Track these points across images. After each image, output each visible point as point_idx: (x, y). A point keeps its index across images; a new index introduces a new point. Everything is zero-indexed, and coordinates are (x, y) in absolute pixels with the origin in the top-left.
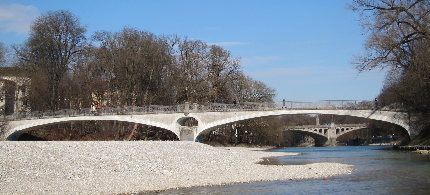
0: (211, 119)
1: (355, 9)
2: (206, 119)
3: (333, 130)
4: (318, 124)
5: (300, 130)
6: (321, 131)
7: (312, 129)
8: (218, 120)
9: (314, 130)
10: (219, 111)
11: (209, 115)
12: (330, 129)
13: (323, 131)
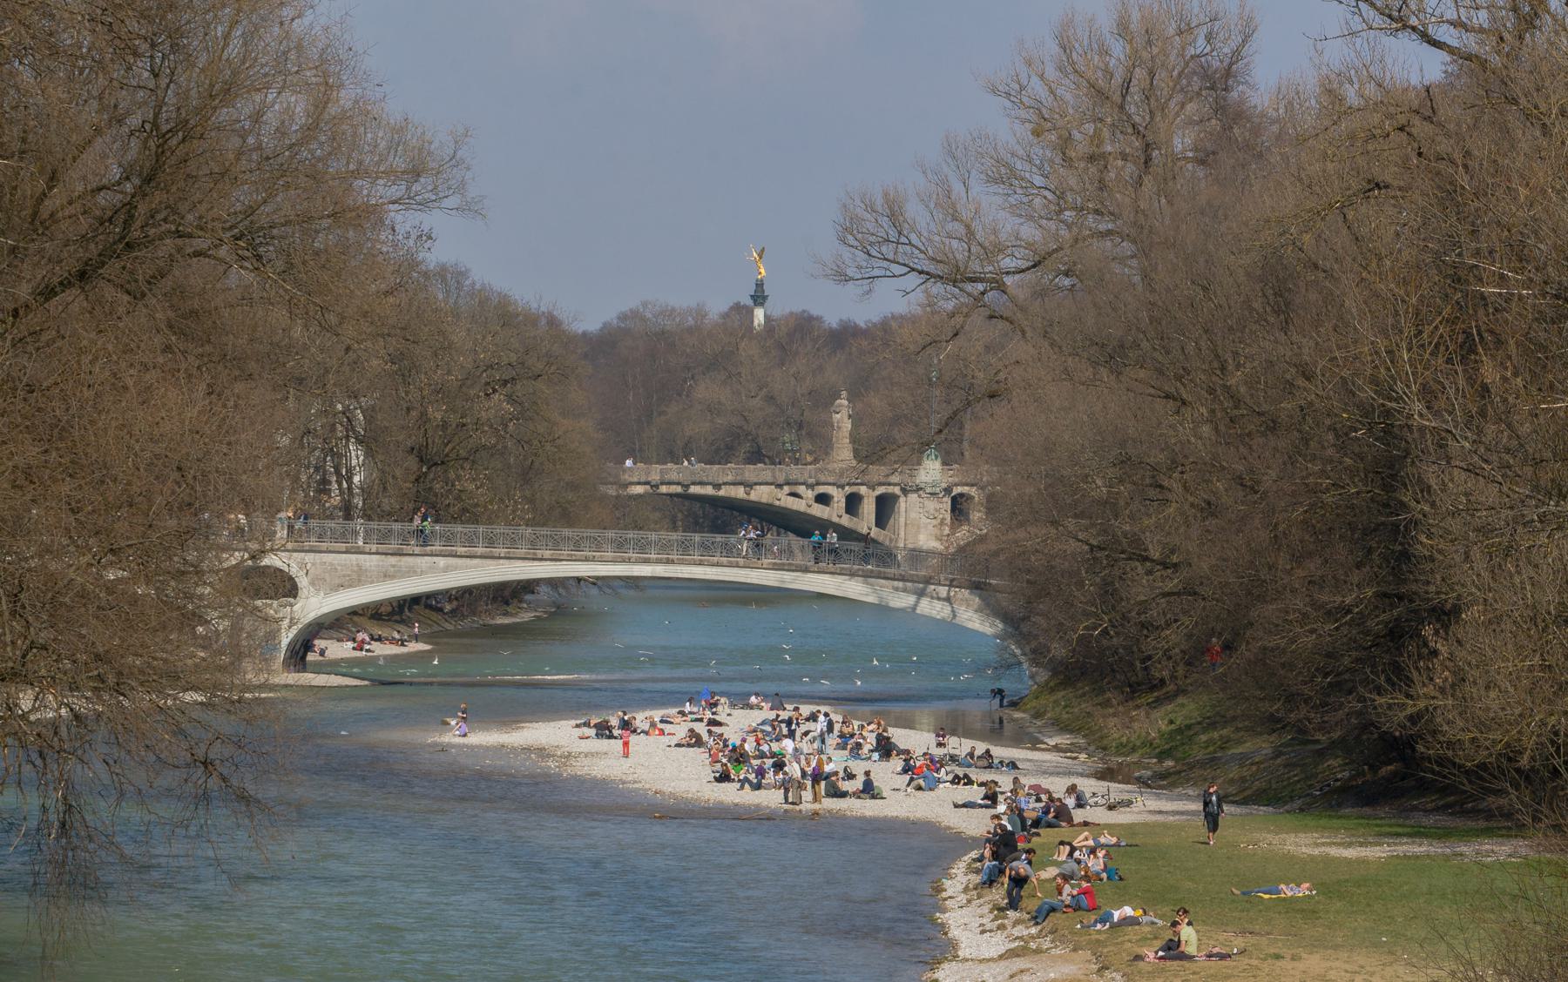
0: (344, 576)
1: (844, 278)
2: (327, 577)
3: (931, 505)
4: (843, 454)
5: (722, 493)
6: (853, 503)
7: (801, 489)
8: (372, 582)
10: (377, 553)
11: (338, 565)
13: (869, 508)
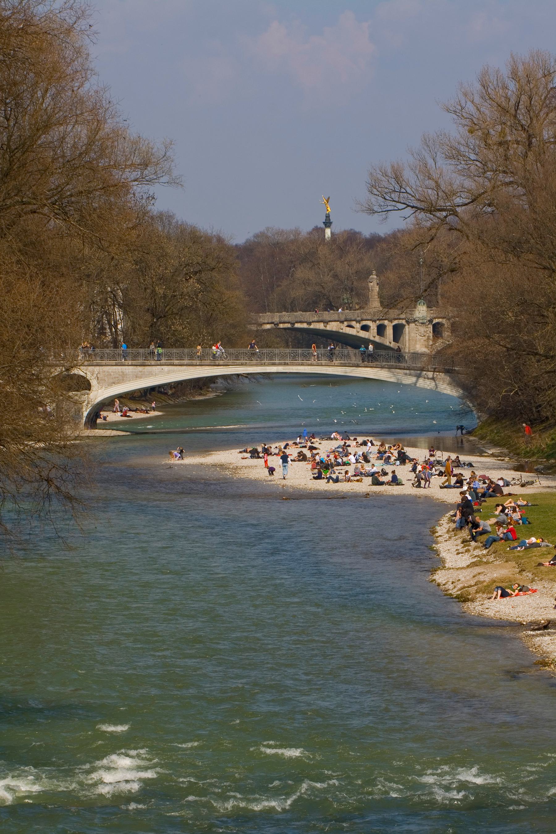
0: (115, 378)
1: (372, 211)
3: (422, 329)
4: (375, 304)
5: (312, 326)
6: (381, 330)
7: (353, 323)
9: (358, 326)
12: (412, 325)
13: (389, 332)
